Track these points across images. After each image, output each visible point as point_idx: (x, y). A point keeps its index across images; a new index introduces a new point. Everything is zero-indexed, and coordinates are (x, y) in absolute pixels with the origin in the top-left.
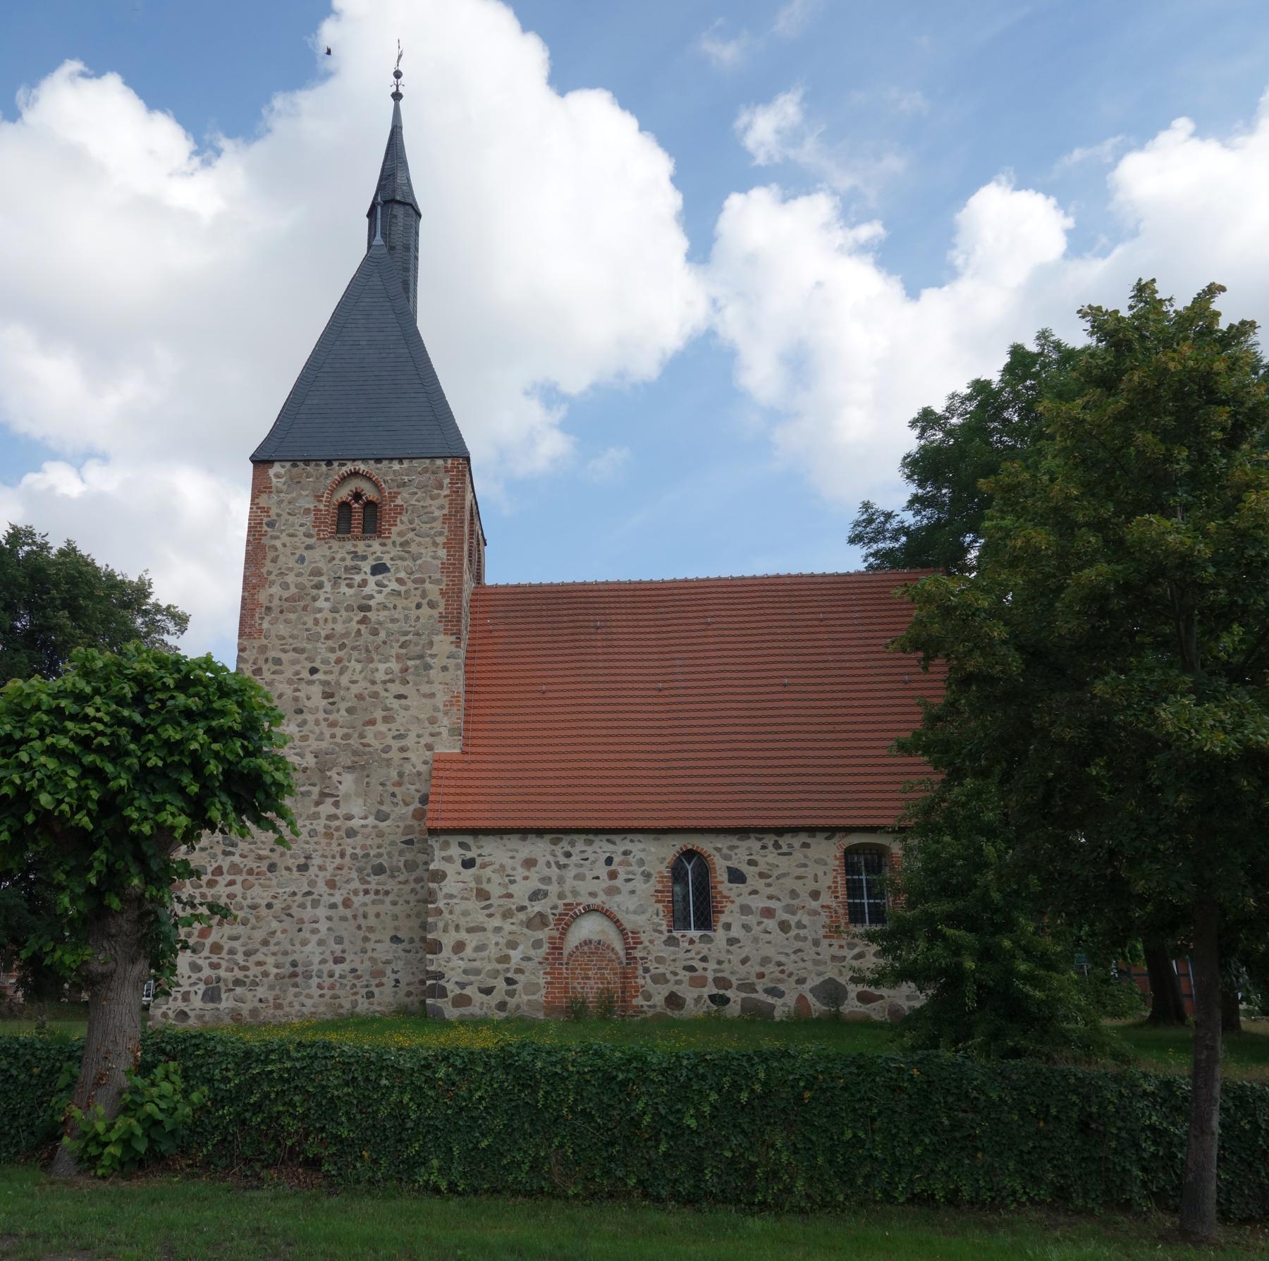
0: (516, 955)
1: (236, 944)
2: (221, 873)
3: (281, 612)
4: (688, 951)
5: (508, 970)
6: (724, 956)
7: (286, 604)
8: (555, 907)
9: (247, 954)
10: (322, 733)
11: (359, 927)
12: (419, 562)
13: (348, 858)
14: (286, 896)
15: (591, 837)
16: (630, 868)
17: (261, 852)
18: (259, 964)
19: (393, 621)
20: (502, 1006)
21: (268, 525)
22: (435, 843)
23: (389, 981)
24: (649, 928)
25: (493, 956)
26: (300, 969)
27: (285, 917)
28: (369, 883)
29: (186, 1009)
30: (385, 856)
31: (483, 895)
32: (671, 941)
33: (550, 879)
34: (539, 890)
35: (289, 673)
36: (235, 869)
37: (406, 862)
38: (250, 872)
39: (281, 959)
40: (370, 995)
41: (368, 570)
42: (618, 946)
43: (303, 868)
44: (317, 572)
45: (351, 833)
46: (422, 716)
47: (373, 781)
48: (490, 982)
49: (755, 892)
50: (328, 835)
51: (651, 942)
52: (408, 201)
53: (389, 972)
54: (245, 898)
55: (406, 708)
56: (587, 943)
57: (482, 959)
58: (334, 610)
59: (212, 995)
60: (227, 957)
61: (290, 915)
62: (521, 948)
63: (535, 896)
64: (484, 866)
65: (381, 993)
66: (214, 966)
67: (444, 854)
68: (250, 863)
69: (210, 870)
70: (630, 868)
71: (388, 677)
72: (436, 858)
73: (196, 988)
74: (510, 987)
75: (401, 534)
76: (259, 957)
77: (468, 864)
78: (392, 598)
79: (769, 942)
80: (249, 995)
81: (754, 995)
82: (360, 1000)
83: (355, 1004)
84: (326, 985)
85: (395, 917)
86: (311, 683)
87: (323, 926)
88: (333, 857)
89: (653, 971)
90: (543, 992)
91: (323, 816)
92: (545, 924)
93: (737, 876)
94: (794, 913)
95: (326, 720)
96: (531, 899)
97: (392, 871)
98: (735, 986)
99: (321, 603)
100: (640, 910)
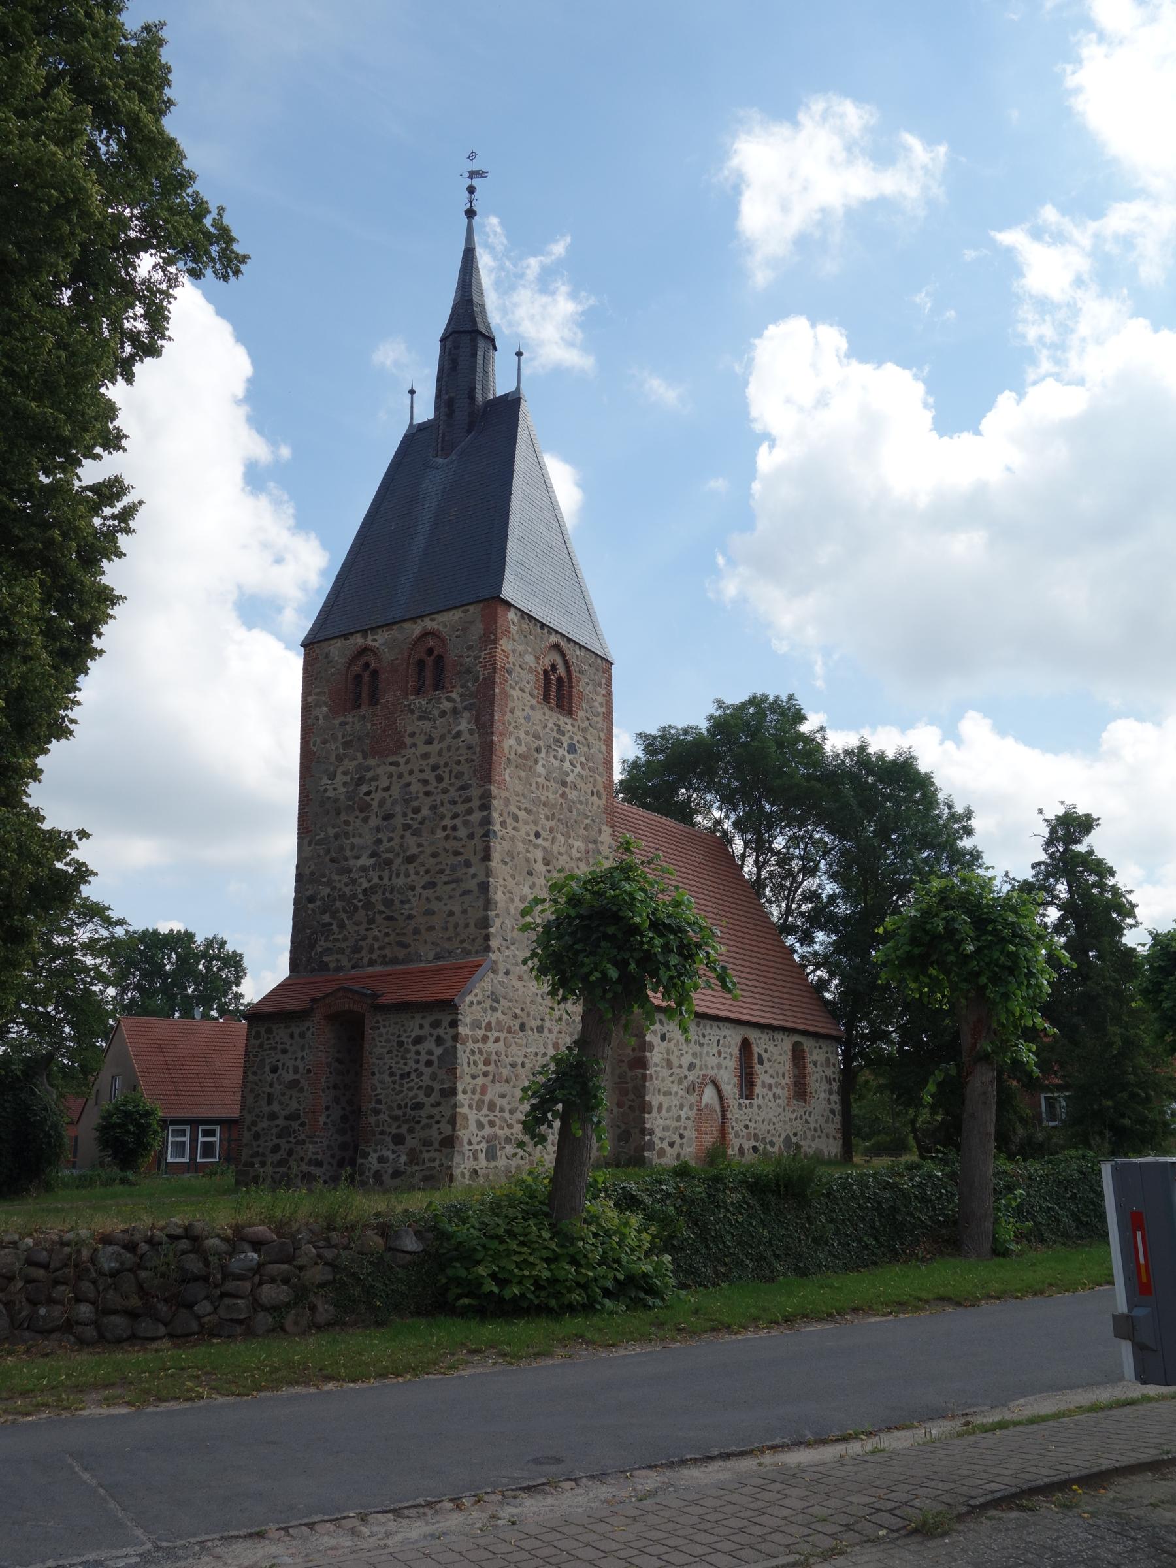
1: (504, 1102)
19: (581, 802)
42: (718, 1108)
54: (507, 1056)
63: (692, 1067)
68: (507, 1020)
69: (484, 1024)
86: (537, 846)
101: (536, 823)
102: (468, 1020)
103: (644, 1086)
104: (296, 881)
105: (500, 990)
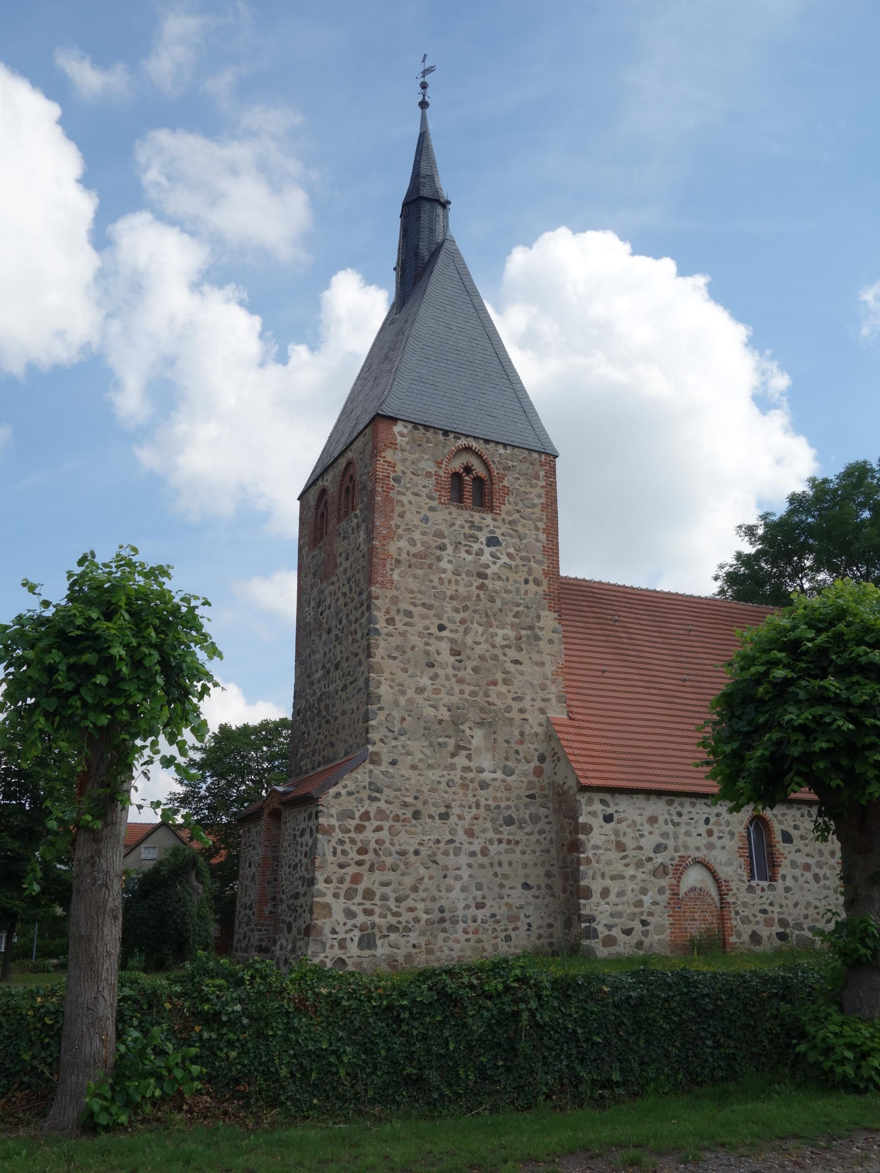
0: (647, 899)
1: (387, 890)
2: (369, 819)
3: (410, 566)
4: (761, 897)
5: (642, 913)
6: (784, 902)
7: (414, 560)
8: (672, 859)
9: (399, 900)
10: (452, 688)
11: (496, 875)
12: (524, 541)
13: (482, 808)
14: (431, 844)
15: (694, 800)
16: (721, 828)
17: (406, 799)
18: (411, 910)
19: (507, 591)
20: (639, 945)
21: (394, 480)
22: (582, 798)
23: (522, 925)
24: (736, 878)
25: (632, 901)
26: (447, 915)
27: (431, 864)
28: (501, 833)
29: (344, 957)
30: (513, 809)
31: (621, 847)
32: (751, 889)
33: (668, 834)
34: (661, 844)
35: (419, 627)
36: (381, 815)
37: (531, 814)
38: (396, 818)
39: (430, 905)
40: (508, 938)
41: (483, 539)
42: (714, 892)
43: (445, 816)
44: (439, 534)
45: (484, 785)
46: (535, 682)
47: (500, 739)
48: (630, 924)
49: (798, 851)
50: (465, 786)
51: (738, 889)
52: (436, 198)
53: (522, 916)
54: (392, 844)
55: (522, 674)
56: (693, 889)
57: (623, 904)
58: (456, 573)
59: (367, 942)
60: (379, 903)
61: (436, 862)
62: (650, 894)
63: (659, 848)
64: (620, 821)
65: (517, 936)
66: (368, 912)
67: (589, 809)
68: (396, 809)
69: (357, 815)
70: (721, 828)
71: (506, 643)
72: (583, 812)
73: (351, 935)
74: (645, 929)
75: (509, 513)
76: (410, 903)
77: (608, 819)
78: (505, 570)
79: (809, 890)
80: (402, 941)
81: (803, 933)
82: (500, 944)
83: (495, 947)
84: (471, 930)
85: (525, 866)
86: (440, 639)
87: (465, 873)
88: (470, 807)
89: (741, 914)
90: (668, 931)
91: (459, 767)
92: (666, 873)
93: (787, 838)
94: (821, 868)
95: (455, 676)
96: (655, 852)
97: (520, 823)
98: (791, 925)
99: (444, 564)
100: (729, 864)
101: (439, 616)
102: (333, 811)
103: (579, 870)
104: (295, 698)
105: (382, 780)
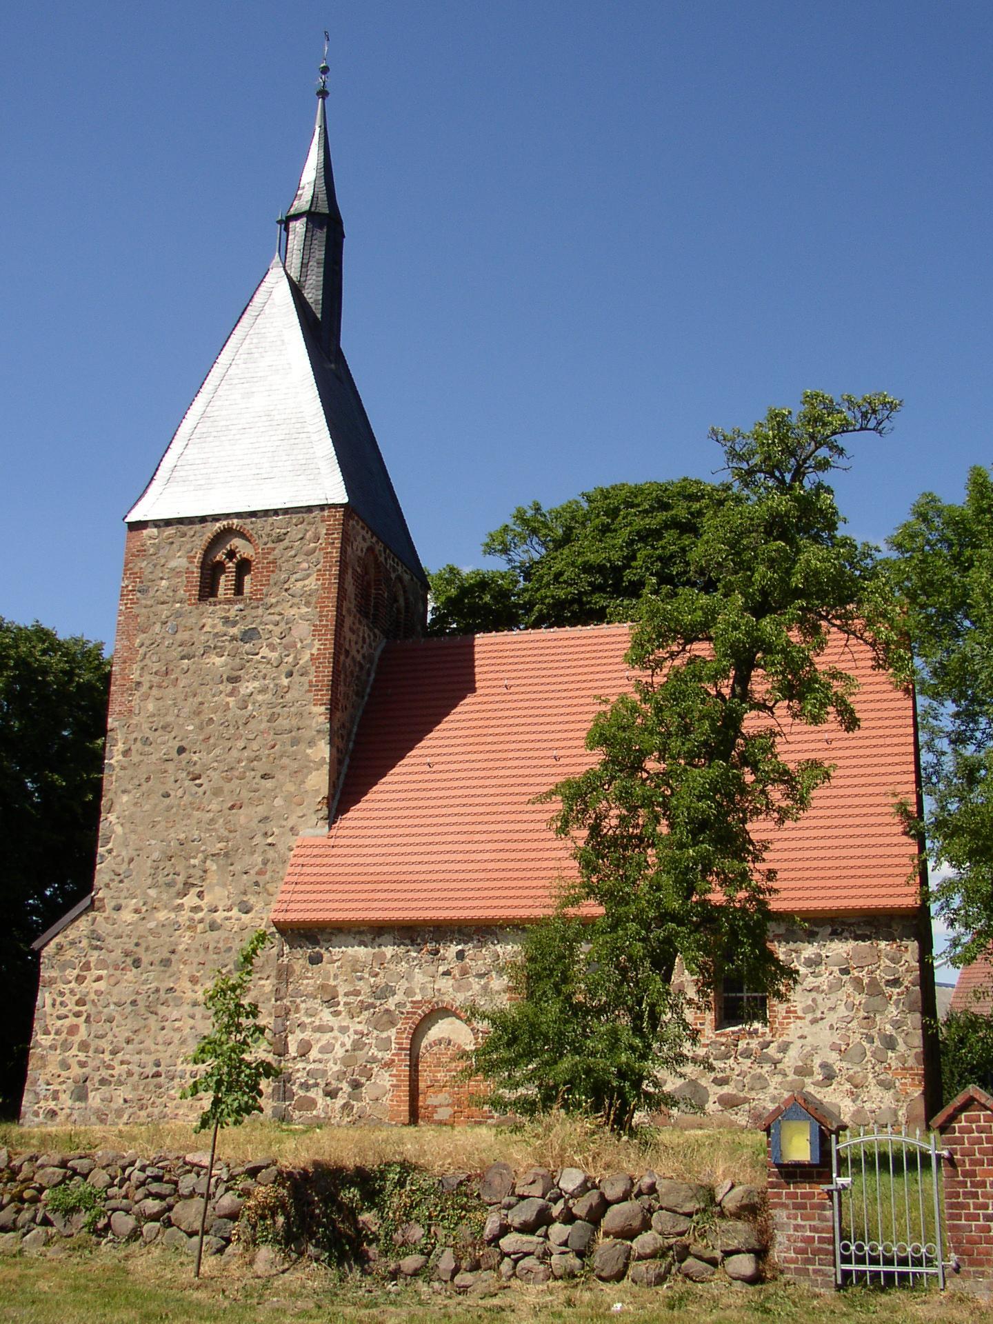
2: (89, 969)
45: (213, 927)
66: (82, 1065)
